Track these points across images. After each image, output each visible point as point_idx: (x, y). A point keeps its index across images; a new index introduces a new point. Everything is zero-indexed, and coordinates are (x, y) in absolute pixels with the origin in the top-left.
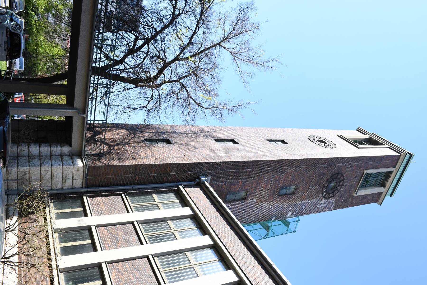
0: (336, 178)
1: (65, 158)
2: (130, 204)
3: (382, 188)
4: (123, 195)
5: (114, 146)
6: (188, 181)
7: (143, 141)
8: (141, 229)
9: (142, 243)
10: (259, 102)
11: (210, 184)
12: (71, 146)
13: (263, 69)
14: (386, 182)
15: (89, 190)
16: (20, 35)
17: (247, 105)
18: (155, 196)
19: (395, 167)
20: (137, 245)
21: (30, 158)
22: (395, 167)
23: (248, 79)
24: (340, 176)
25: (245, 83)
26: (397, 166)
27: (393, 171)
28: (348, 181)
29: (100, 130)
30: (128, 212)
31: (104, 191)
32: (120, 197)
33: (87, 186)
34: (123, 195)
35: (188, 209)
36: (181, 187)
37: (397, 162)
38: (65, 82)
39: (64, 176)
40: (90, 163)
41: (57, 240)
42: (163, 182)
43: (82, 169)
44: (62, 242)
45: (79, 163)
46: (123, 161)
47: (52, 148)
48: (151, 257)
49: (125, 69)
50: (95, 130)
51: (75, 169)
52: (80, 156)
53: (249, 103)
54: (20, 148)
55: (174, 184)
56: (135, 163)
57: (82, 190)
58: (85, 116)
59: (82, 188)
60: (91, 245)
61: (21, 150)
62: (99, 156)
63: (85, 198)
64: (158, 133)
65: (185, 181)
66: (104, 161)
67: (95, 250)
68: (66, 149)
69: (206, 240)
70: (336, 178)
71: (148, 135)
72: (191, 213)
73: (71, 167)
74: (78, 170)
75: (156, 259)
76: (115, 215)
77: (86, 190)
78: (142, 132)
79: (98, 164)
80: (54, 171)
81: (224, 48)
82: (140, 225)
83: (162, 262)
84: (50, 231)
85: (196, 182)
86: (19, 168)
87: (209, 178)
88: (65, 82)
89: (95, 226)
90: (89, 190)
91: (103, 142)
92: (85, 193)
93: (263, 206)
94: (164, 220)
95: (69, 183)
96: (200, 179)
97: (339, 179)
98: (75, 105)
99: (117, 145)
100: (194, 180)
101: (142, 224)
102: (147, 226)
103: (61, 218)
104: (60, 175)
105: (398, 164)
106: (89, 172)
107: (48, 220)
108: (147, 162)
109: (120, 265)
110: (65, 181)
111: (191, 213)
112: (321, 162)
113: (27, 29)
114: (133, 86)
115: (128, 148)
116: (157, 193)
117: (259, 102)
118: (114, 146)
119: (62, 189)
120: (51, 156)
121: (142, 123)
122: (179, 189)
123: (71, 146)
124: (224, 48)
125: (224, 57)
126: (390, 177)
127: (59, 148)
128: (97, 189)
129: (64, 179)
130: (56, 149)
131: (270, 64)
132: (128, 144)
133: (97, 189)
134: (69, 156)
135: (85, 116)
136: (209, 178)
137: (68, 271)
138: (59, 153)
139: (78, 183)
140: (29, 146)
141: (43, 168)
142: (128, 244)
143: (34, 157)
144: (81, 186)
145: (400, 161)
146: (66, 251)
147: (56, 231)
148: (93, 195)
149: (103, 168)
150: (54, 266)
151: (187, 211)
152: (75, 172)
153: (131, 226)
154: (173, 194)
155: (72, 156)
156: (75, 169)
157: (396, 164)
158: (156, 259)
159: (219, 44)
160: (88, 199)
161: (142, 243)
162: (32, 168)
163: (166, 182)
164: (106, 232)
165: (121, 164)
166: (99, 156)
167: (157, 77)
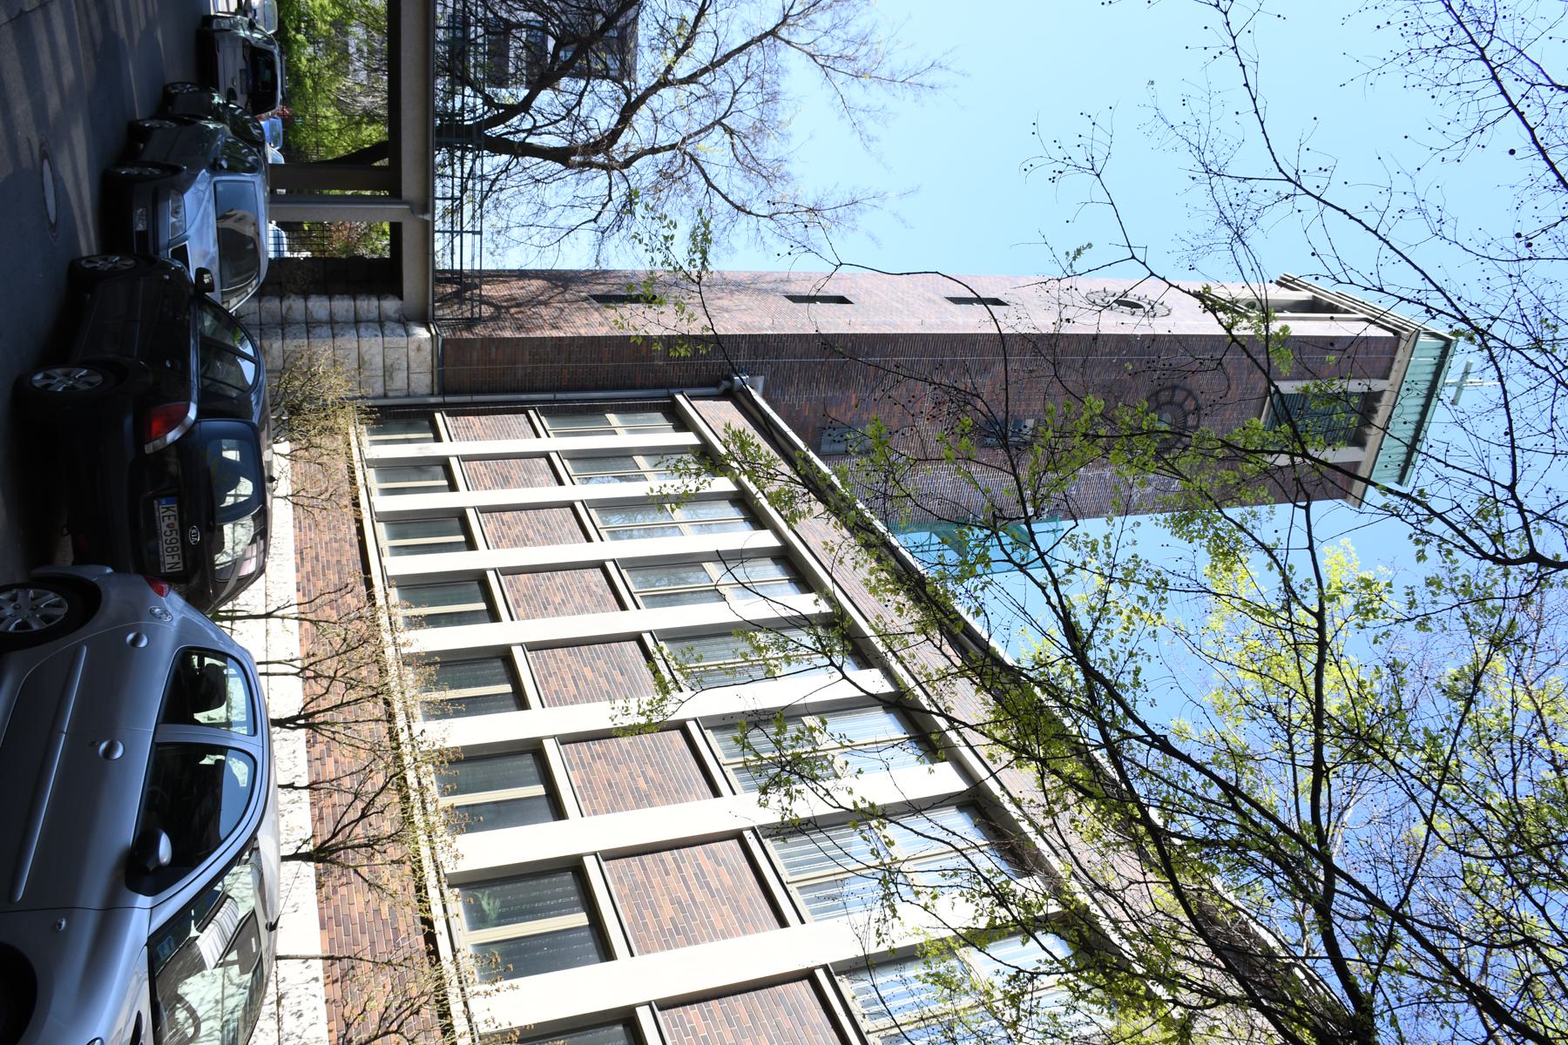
0: (1170, 403)
1: (388, 325)
2: (633, 589)
3: (1356, 449)
4: (531, 413)
5: (508, 308)
6: (701, 385)
7: (585, 299)
8: (716, 747)
9: (716, 793)
10: (915, 191)
11: (764, 397)
12: (401, 298)
13: (910, 94)
14: (1367, 431)
15: (448, 399)
16: (272, 54)
17: (875, 201)
18: (611, 417)
19: (1386, 377)
21: (310, 325)
22: (1386, 377)
23: (871, 127)
24: (1180, 396)
25: (868, 140)
26: (1393, 375)
27: (1382, 392)
29: (477, 281)
30: (783, 923)
31: (484, 403)
32: (522, 417)
33: (444, 392)
34: (531, 413)
35: (945, 769)
36: (680, 398)
37: (1392, 360)
38: (385, 162)
39: (388, 362)
40: (446, 334)
42: (633, 388)
43: (428, 347)
44: (380, 481)
45: (422, 333)
46: (528, 330)
48: (579, 506)
49: (535, 127)
50: (464, 283)
51: (413, 347)
52: (425, 322)
53: (881, 196)
54: (286, 304)
55: (663, 392)
56: (555, 333)
57: (433, 400)
58: (428, 217)
59: (432, 395)
60: (587, 933)
61: (290, 308)
62: (470, 323)
63: (438, 416)
64: (630, 287)
65: (692, 386)
66: (480, 331)
67: (607, 954)
68: (390, 305)
69: (946, 779)
70: (1170, 403)
71: (600, 289)
72: (960, 785)
73: (403, 341)
74: (419, 349)
75: (845, 985)
76: (729, 941)
77: (439, 400)
78: (586, 283)
79: (466, 335)
80: (363, 350)
81: (788, 43)
82: (709, 733)
83: (789, 856)
84: (357, 465)
85: (722, 388)
86: (288, 341)
87: (760, 380)
88: (385, 162)
89: (649, 1004)
90: (448, 399)
91: (484, 301)
93: (937, 478)
94: (693, 561)
95: (399, 381)
96: (732, 380)
97: (1181, 405)
98: (404, 194)
99: (518, 305)
100: (716, 384)
101: (713, 729)
102: (580, 464)
103: (471, 828)
104: (378, 361)
105: (1396, 366)
106: (447, 356)
107: (440, 926)
108: (583, 332)
109: (507, 516)
110: (391, 377)
111: (960, 785)
112: (1105, 346)
114: (558, 166)
115: (543, 311)
116: (617, 410)
117: (915, 191)
118: (508, 308)
119: (385, 396)
120: (357, 322)
121: (592, 266)
122: (676, 403)
123: (401, 298)
124: (788, 43)
125: (795, 71)
126: (1376, 411)
127: (374, 302)
128: (467, 399)
129: (388, 372)
130: (368, 306)
131: (927, 79)
132: (546, 304)
133: (467, 399)
134: (398, 321)
135: (428, 217)
136: (760, 380)
137: (471, 883)
138: (374, 314)
139: (422, 382)
140: (306, 300)
141: (339, 341)
142: (670, 794)
143: (319, 323)
144: (428, 391)
145: (1399, 356)
146: (440, 711)
148: (455, 411)
149: (478, 345)
150: (356, 457)
151: (946, 779)
152: (412, 354)
155: (405, 321)
156: (413, 347)
157: (1390, 369)
158: (845, 985)
159: (773, 33)
160: (603, 864)
161: (716, 793)
162: (316, 342)
163: (642, 388)
164: (483, 469)
165: (523, 335)
166: (470, 323)
167: (614, 135)
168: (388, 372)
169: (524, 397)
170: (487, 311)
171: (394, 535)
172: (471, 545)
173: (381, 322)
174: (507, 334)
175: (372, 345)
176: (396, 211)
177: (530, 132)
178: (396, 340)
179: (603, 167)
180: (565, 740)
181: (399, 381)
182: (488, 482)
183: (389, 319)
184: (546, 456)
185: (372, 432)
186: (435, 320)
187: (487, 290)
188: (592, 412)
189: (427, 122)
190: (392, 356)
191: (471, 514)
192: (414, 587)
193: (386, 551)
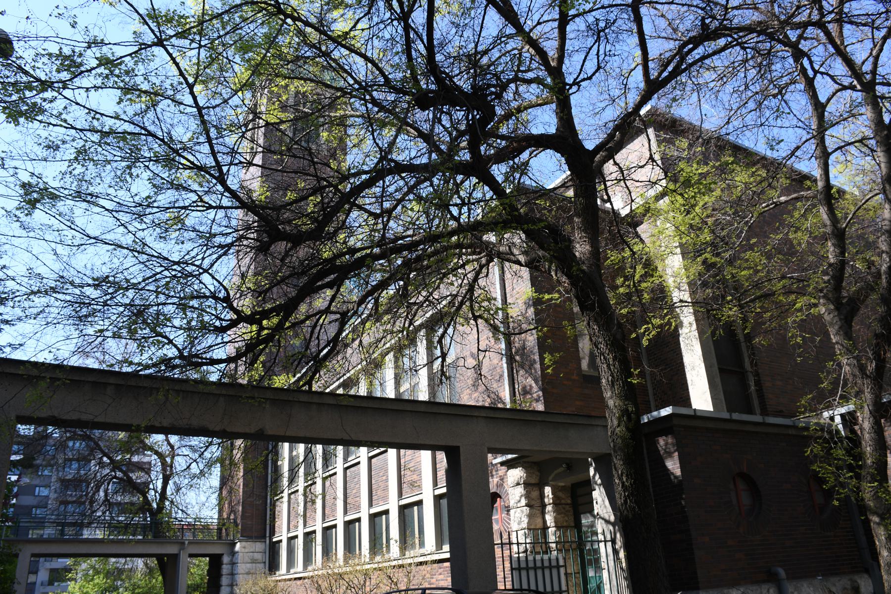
15: (268, 535)
20: (359, 469)
28: (3, 208)
33: (264, 537)
41: (412, 553)
43: (244, 543)
45: (238, 547)
47: (239, 572)
48: (346, 465)
51: (243, 550)
63: (274, 540)
68: (226, 559)
73: (241, 555)
77: (268, 539)
90: (268, 535)
91: (228, 518)
92: (271, 539)
95: (258, 556)
104: (248, 565)
106: (249, 535)
107: (422, 559)
113: (269, 236)
120: (232, 574)
127: (224, 566)
128: (268, 527)
129: (254, 561)
130: (225, 569)
133: (268, 527)
134: (233, 556)
138: (229, 567)
139: (259, 546)
147: (371, 559)
148: (273, 533)
153: (373, 460)
154: (549, 152)
155: (233, 553)
156: (243, 550)
168: (254, 561)
169: (269, 501)
170: (232, 517)
171: (413, 546)
172: (419, 503)
173: (233, 564)
174: (240, 509)
175: (241, 568)
176: (184, 559)
177: (156, 492)
178: (240, 558)
179: (173, 458)
180: (371, 505)
181: (258, 556)
182: (358, 499)
183: (232, 560)
184: (346, 469)
185: (278, 570)
186: (233, 540)
187: (225, 515)
188: (277, 470)
189: (150, 542)
190: (247, 559)
191: (325, 525)
192: (404, 543)
193: (422, 551)
